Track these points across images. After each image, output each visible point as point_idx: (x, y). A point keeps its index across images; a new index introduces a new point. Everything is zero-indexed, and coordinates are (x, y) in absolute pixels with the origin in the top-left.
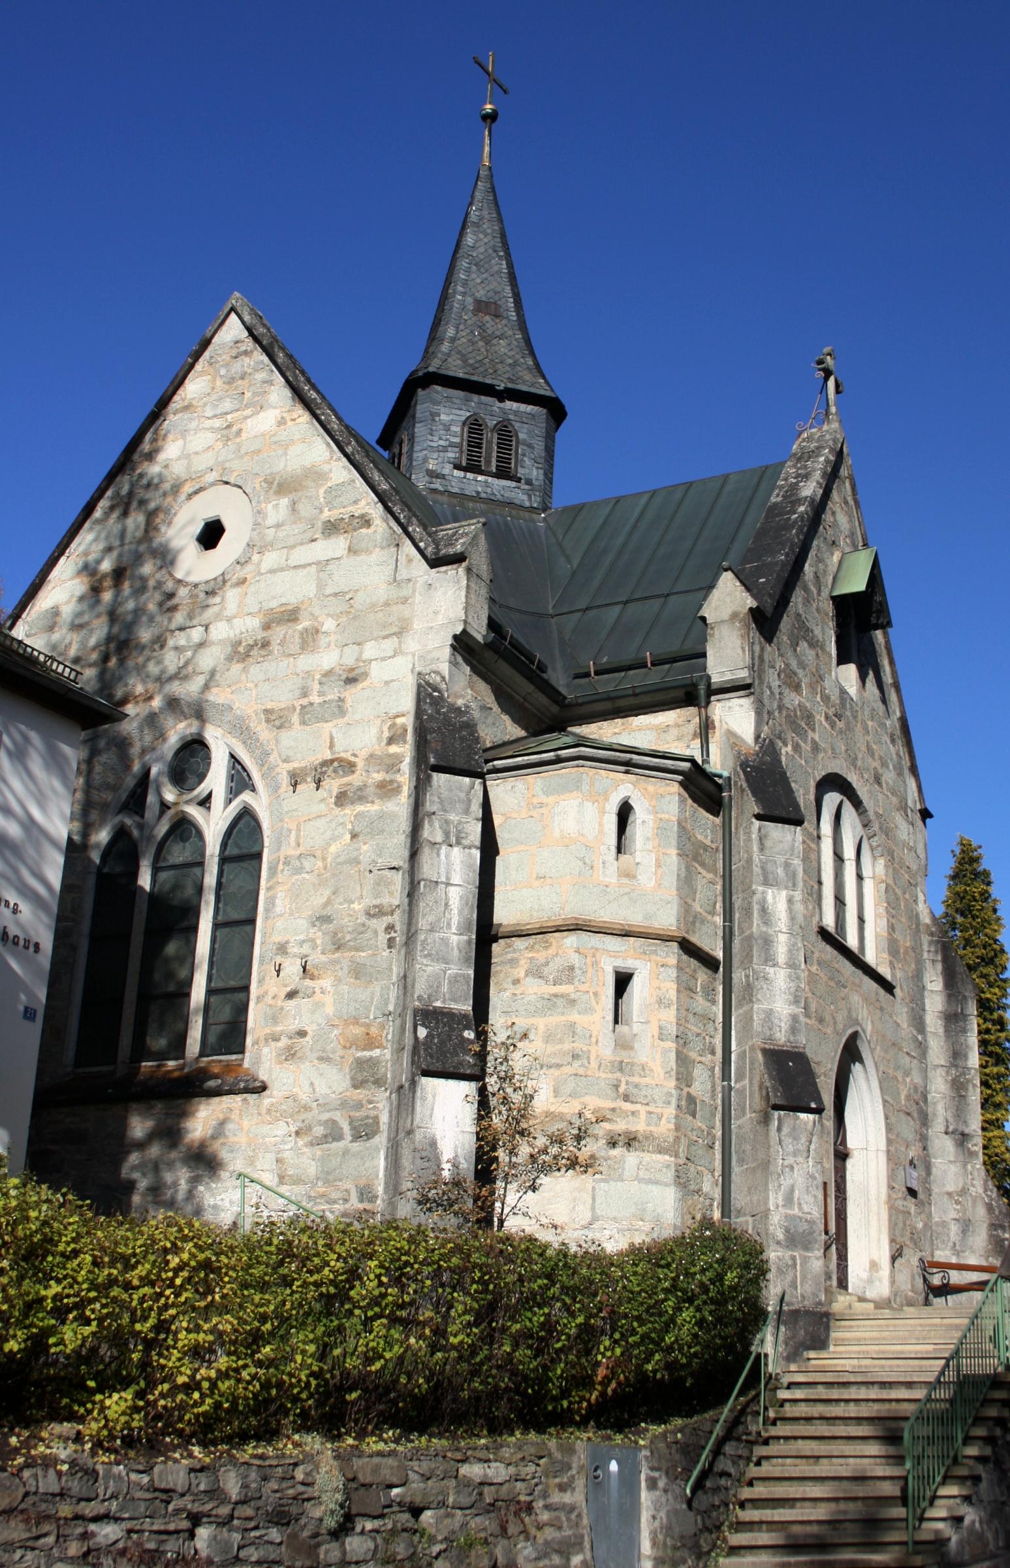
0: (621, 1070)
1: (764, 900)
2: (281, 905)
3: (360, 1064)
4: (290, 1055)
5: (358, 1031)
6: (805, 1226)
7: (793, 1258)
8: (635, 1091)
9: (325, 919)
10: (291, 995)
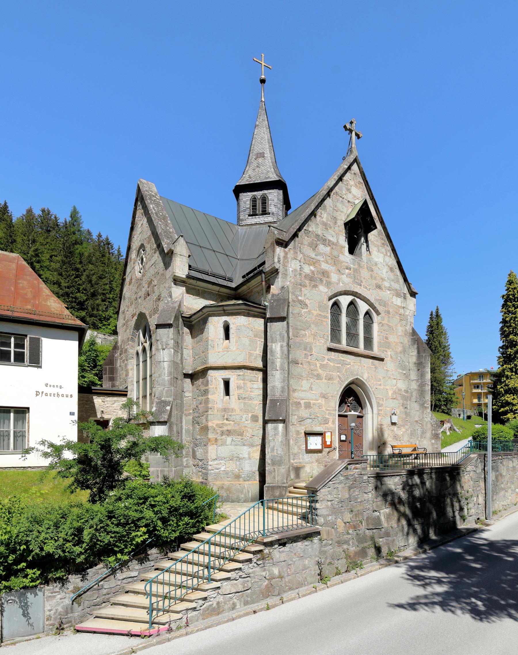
0: (225, 411)
1: (272, 348)
6: (279, 458)
7: (274, 469)
8: (230, 417)
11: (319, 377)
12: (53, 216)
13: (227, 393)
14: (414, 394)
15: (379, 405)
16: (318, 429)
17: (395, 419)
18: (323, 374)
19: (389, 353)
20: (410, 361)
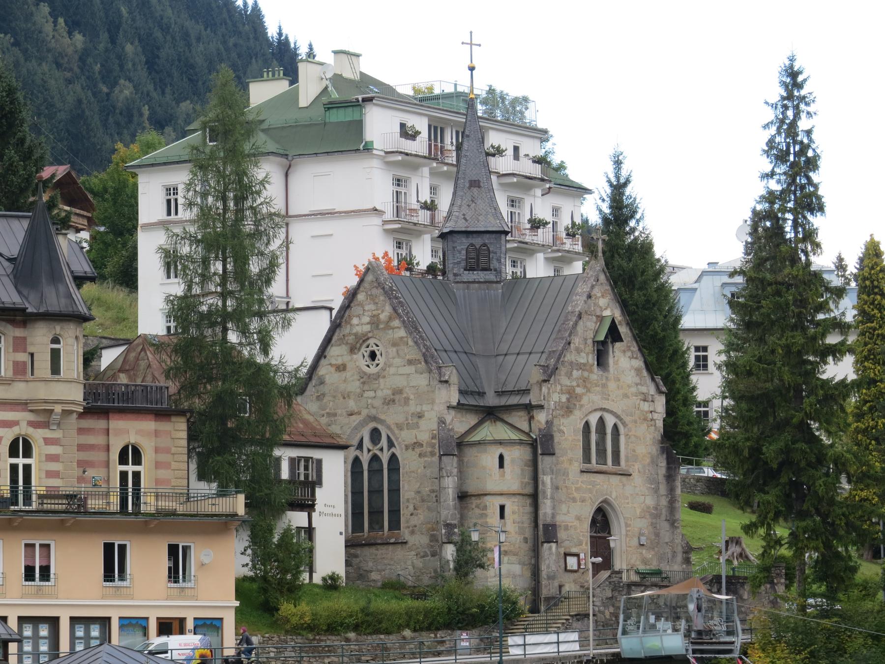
2: (406, 487)
3: (432, 536)
4: (413, 533)
5: (430, 526)
9: (419, 492)
10: (412, 515)
11: (574, 500)
12: (449, 417)
13: (502, 516)
14: (664, 512)
15: (627, 525)
16: (574, 550)
17: (643, 540)
18: (576, 495)
19: (636, 467)
20: (659, 472)
